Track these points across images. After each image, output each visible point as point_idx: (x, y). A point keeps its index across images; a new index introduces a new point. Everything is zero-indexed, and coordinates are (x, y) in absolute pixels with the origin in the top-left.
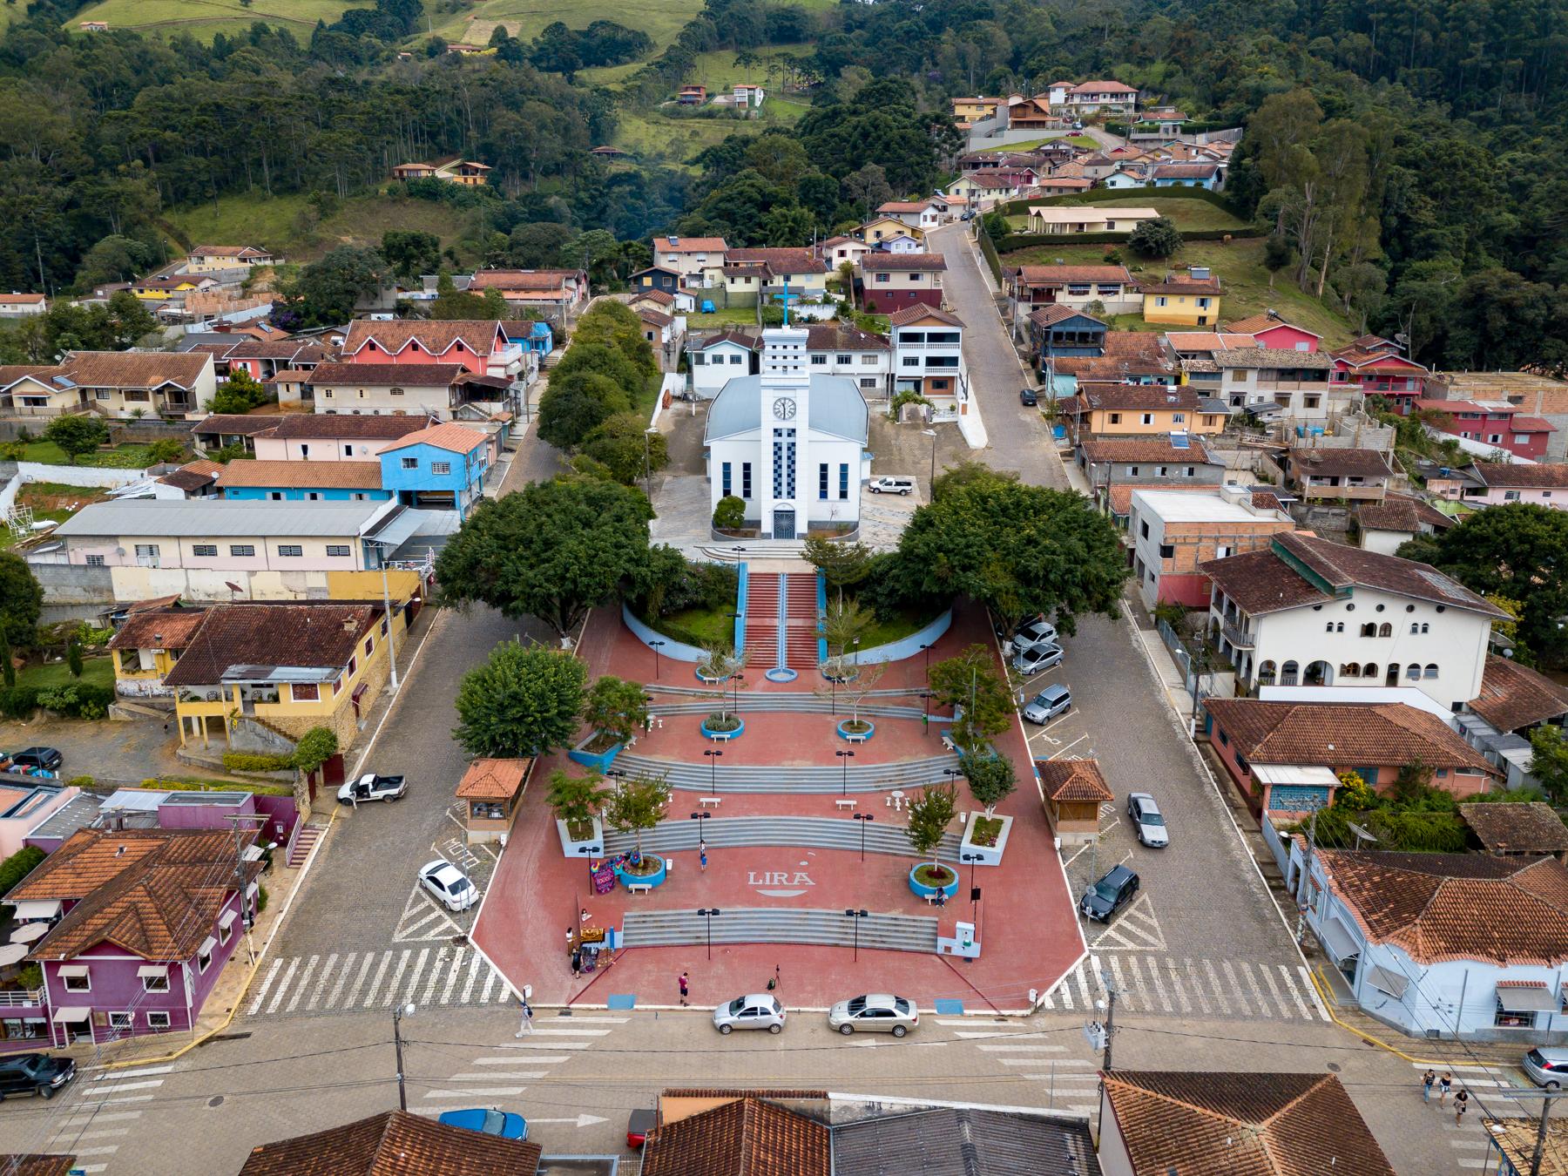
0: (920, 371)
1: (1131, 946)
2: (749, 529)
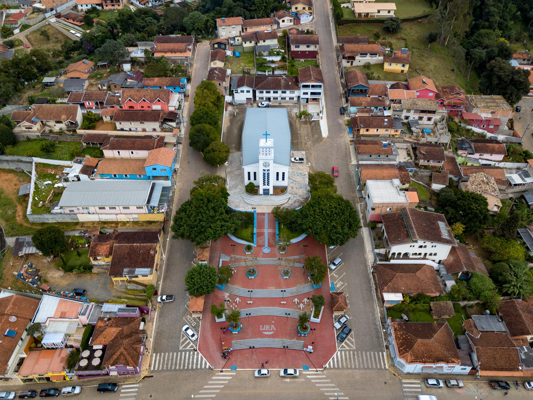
0: (309, 96)
1: (347, 348)
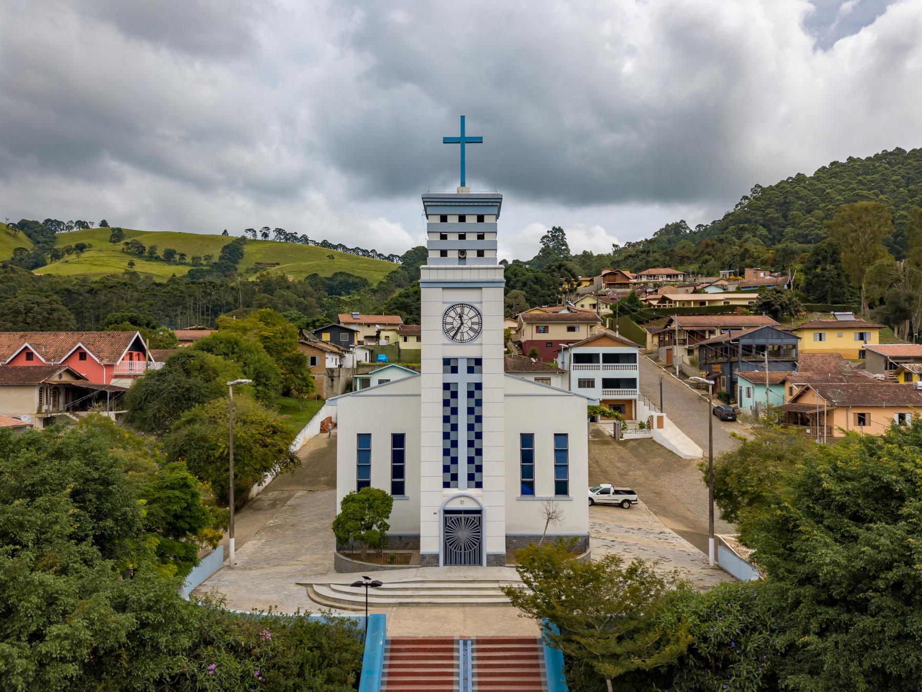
2: (404, 550)
